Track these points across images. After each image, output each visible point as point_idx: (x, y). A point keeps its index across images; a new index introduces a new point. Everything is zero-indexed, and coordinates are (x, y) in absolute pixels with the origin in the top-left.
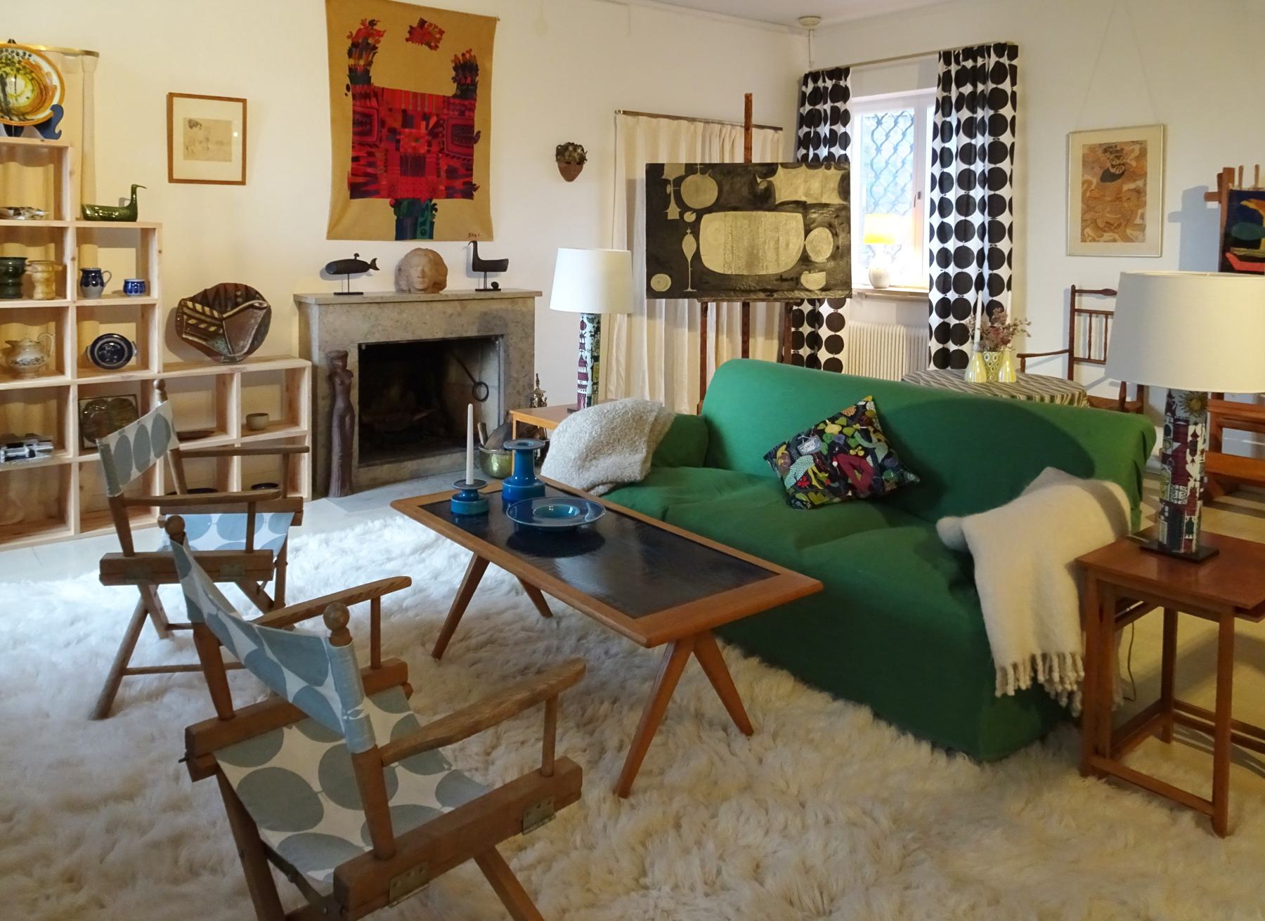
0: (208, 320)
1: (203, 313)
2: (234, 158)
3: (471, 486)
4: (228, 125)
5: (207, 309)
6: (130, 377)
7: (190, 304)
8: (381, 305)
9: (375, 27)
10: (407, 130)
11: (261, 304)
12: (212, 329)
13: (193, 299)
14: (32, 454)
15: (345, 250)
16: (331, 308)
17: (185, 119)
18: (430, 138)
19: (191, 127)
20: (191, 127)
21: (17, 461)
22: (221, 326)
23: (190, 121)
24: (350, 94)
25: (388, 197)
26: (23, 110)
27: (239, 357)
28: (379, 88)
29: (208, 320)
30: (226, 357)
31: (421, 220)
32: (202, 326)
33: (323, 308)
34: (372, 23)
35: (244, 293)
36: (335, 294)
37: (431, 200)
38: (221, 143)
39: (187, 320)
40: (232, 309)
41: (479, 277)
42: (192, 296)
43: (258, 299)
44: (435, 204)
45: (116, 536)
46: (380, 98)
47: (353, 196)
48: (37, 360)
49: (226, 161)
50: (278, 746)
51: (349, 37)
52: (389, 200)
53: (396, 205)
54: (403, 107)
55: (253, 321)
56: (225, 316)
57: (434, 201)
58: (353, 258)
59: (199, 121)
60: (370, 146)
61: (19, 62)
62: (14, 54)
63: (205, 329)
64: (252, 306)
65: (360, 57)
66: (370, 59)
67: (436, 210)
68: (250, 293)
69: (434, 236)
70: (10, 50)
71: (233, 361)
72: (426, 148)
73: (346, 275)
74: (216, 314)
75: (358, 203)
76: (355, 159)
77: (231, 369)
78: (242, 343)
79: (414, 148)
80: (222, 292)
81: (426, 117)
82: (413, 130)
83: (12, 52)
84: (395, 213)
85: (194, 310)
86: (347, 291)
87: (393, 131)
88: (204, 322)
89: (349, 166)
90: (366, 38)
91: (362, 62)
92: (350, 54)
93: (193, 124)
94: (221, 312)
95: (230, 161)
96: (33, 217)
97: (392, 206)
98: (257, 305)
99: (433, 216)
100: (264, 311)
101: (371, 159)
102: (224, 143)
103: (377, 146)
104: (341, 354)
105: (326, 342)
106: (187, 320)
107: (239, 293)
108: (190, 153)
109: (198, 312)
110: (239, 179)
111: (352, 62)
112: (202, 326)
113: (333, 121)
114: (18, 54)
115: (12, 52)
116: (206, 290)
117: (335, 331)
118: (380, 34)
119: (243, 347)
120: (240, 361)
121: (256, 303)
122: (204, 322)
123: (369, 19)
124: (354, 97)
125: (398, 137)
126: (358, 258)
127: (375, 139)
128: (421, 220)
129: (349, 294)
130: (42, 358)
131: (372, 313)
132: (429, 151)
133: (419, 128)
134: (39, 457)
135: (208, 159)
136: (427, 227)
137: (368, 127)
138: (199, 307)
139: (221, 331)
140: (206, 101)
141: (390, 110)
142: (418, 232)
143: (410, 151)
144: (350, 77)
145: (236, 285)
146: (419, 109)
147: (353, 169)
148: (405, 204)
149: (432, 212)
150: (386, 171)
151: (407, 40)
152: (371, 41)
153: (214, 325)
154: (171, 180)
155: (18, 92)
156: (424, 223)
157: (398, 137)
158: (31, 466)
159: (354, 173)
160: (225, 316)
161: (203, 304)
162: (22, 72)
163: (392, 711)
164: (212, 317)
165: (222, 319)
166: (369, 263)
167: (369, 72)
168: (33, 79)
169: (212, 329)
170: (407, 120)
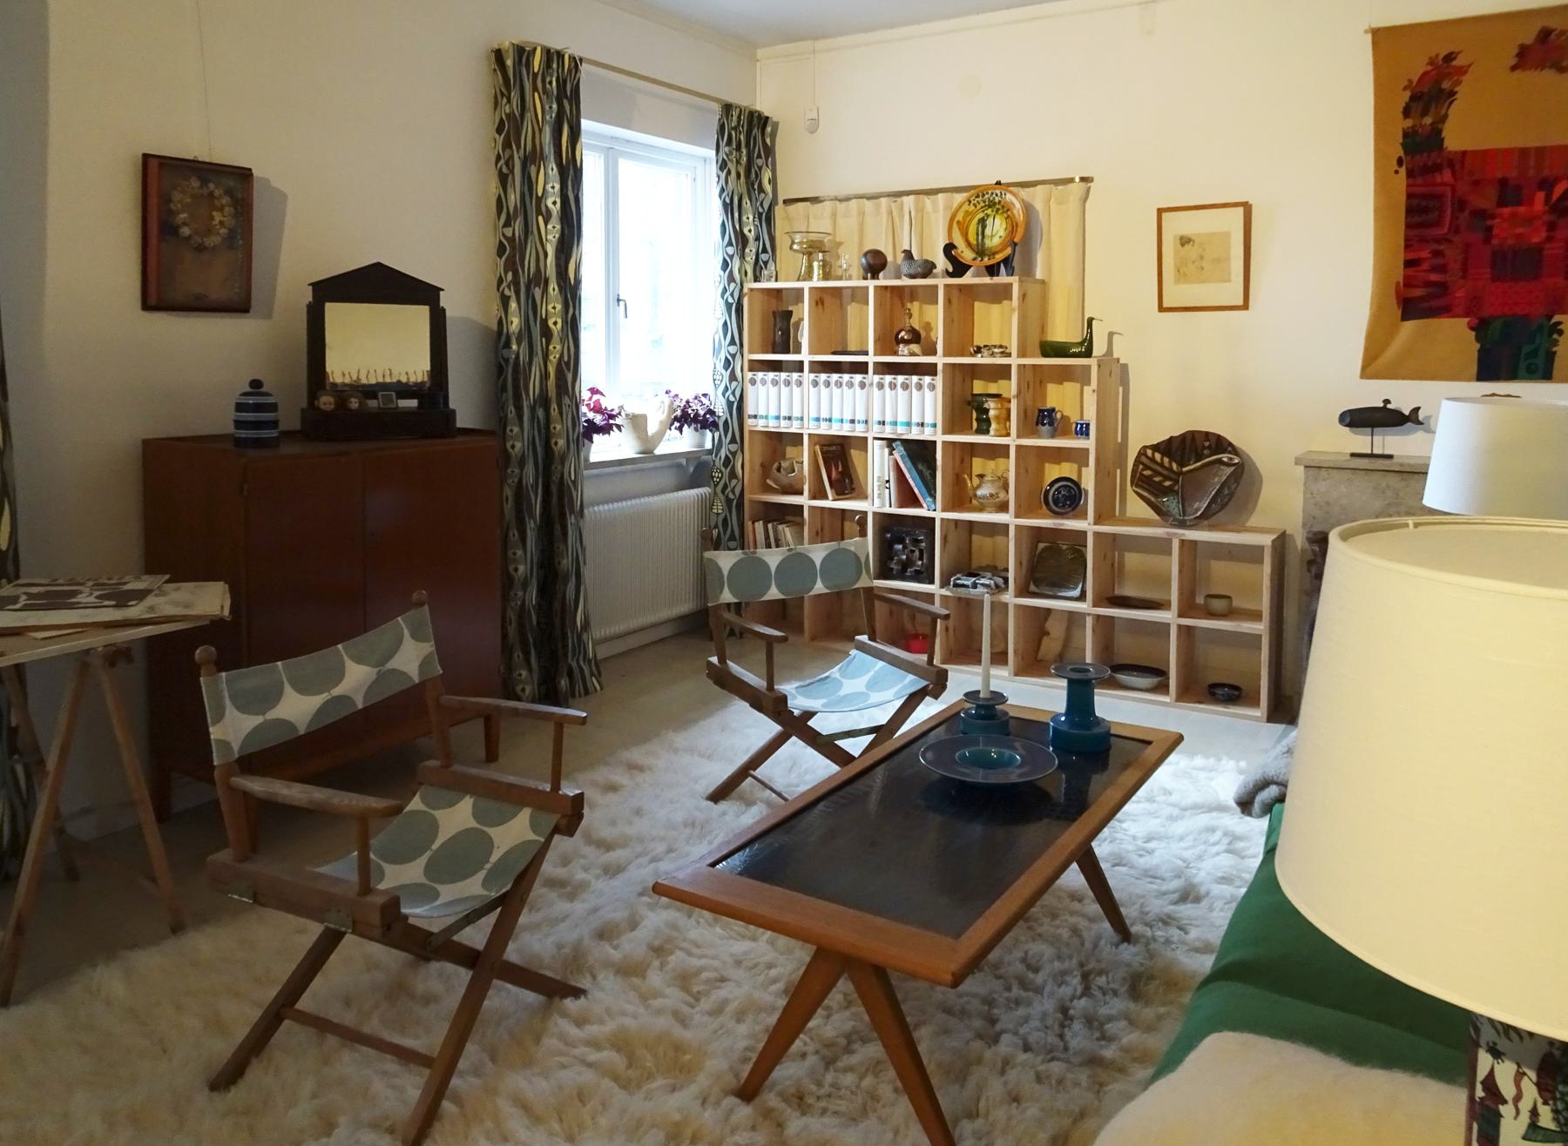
0: (1165, 472)
1: (1161, 465)
2: (1233, 277)
3: (985, 699)
4: (1226, 236)
5: (1166, 460)
6: (1063, 524)
7: (1149, 452)
8: (1405, 476)
9: (1454, 63)
10: (1506, 211)
11: (1231, 459)
12: (1167, 483)
13: (1155, 448)
14: (975, 586)
15: (1372, 394)
16: (1323, 473)
17: (1175, 236)
18: (1552, 217)
19: (1183, 245)
20: (1183, 245)
21: (962, 589)
22: (1176, 482)
23: (1182, 238)
24: (1403, 171)
25: (1466, 315)
26: (994, 250)
27: (1191, 520)
28: (1456, 152)
29: (1165, 472)
30: (1175, 520)
31: (1527, 349)
32: (1157, 479)
33: (1312, 471)
34: (1449, 58)
35: (1213, 446)
36: (1353, 455)
37: (1551, 317)
38: (1218, 261)
39: (1143, 470)
40: (1194, 463)
41: (1367, 435)
42: (1155, 443)
43: (1230, 453)
44: (1560, 323)
45: (1065, 693)
46: (1457, 166)
47: (1405, 317)
48: (992, 495)
49: (1225, 281)
50: (451, 804)
51: (1405, 89)
52: (1466, 320)
53: (1480, 328)
54: (1499, 175)
55: (1216, 479)
56: (1185, 469)
57: (1556, 318)
58: (1382, 405)
59: (1193, 238)
60: (1438, 241)
61: (1000, 202)
62: (994, 195)
63: (1160, 483)
64: (1220, 461)
65: (1424, 113)
66: (1443, 112)
67: (1561, 333)
68: (1220, 444)
69: (1555, 373)
70: (990, 192)
71: (1182, 524)
72: (1544, 234)
73: (1369, 430)
74: (1175, 466)
75: (1410, 326)
76: (1409, 264)
77: (1168, 533)
78: (1196, 505)
79: (1519, 236)
80: (1188, 442)
81: (1546, 184)
82: (1522, 209)
83: (992, 194)
84: (1478, 339)
85: (1153, 460)
86: (1369, 452)
87: (1481, 214)
88: (1159, 474)
89: (1399, 273)
90: (1438, 82)
91: (1428, 120)
92: (1407, 113)
93: (1185, 241)
94: (1181, 465)
95: (1230, 281)
96: (992, 355)
97: (1472, 328)
98: (1225, 460)
99: (1555, 343)
100: (1232, 469)
101: (1439, 261)
102: (1222, 261)
103: (1449, 241)
104: (1320, 537)
105: (1314, 518)
106: (1143, 470)
107: (1207, 444)
108: (1181, 276)
109: (1156, 463)
110: (1165, 305)
111: (1409, 123)
112: (1157, 479)
113: (1376, 211)
114: (997, 195)
115: (992, 194)
116: (1171, 437)
117: (1328, 503)
118: (1463, 71)
119: (1197, 510)
120: (1188, 526)
121: (1225, 457)
122: (1159, 474)
123: (1443, 53)
124: (1410, 174)
125: (1489, 222)
126: (1389, 406)
127: (1446, 230)
128: (1527, 349)
129: (1372, 456)
130: (997, 494)
131: (1388, 486)
132: (1549, 239)
133: (1531, 202)
134: (980, 590)
135: (1203, 282)
136: (1540, 361)
137: (1437, 213)
138: (1158, 456)
139: (1176, 488)
140: (1205, 211)
141: (1476, 183)
142: (1523, 365)
143: (1510, 242)
144: (1404, 145)
145: (1207, 434)
146: (1531, 173)
147: (1406, 277)
148: (1496, 326)
149: (1550, 335)
150: (1464, 277)
151: (1514, 68)
152: (1446, 85)
153: (1170, 479)
154: (1161, 309)
155: (994, 233)
156: (1534, 353)
157: (1489, 222)
158: (971, 597)
159: (1408, 283)
160: (1185, 469)
161: (1163, 454)
162: (1000, 212)
163: (534, 832)
164: (1170, 469)
165: (1181, 473)
166: (1407, 413)
167: (1440, 131)
168: (1008, 216)
169: (1167, 483)
170: (1509, 192)
